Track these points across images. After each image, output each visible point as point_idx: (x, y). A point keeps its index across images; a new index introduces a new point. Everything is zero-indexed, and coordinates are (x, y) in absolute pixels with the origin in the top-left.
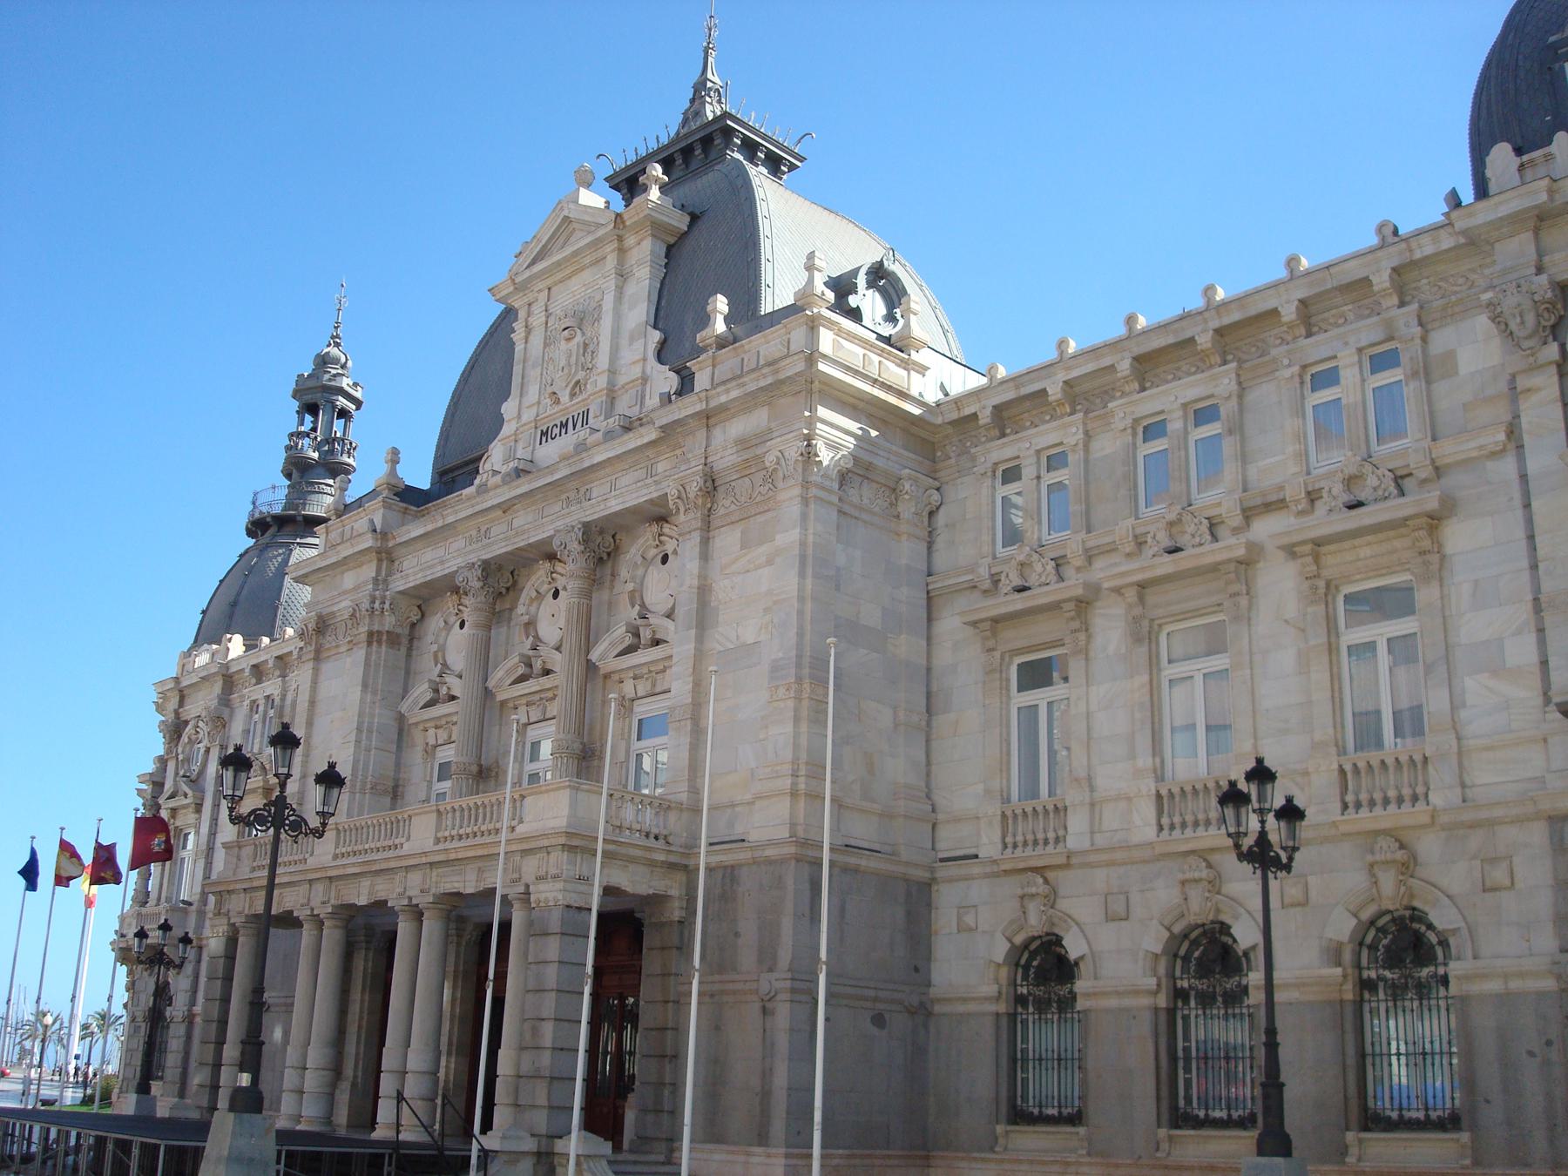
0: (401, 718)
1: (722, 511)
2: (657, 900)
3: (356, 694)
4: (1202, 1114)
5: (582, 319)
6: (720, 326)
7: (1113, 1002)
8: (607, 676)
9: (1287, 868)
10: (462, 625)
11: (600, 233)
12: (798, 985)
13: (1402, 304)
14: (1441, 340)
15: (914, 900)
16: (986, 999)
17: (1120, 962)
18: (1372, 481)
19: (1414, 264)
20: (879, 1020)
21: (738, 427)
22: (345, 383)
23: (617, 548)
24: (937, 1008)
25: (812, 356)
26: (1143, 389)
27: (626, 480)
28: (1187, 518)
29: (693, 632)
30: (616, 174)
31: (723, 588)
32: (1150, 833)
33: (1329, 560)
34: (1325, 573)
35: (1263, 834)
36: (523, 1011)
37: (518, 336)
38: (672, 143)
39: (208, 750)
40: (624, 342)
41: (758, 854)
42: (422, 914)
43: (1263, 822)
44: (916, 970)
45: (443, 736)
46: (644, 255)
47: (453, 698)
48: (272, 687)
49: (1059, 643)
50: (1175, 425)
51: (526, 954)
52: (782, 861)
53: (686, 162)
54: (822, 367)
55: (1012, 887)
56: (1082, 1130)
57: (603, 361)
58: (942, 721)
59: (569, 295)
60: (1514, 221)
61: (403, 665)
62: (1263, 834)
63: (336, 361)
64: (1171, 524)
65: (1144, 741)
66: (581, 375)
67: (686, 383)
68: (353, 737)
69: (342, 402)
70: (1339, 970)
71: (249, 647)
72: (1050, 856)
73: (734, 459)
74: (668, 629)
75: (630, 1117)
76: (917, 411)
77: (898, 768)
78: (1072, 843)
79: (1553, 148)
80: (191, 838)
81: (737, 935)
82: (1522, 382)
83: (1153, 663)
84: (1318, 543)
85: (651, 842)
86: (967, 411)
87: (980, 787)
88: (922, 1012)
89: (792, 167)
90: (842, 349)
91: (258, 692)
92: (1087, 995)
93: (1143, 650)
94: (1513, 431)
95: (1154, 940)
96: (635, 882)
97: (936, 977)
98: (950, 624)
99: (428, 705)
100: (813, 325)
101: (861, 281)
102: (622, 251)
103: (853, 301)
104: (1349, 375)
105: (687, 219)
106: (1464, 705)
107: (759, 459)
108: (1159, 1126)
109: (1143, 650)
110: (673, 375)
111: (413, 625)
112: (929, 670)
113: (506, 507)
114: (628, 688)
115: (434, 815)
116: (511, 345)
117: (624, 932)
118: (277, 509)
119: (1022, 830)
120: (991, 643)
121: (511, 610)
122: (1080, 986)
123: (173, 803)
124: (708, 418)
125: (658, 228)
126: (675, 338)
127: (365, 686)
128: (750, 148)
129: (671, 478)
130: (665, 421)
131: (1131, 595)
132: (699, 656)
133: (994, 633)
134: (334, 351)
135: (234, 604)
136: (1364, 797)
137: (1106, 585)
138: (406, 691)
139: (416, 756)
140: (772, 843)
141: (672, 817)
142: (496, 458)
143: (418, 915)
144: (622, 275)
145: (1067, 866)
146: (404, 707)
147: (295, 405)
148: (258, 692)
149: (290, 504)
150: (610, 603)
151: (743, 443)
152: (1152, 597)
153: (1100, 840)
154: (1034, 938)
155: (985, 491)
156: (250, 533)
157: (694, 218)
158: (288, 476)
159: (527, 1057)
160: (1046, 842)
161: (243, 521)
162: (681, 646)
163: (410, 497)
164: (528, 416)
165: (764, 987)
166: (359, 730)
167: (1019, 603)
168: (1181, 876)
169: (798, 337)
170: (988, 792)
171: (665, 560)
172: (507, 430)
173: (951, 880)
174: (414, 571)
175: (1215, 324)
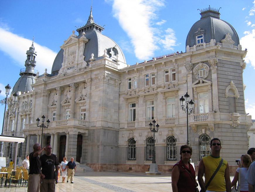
0: (48, 107)
1: (93, 83)
2: (85, 133)
3: (42, 104)
4: (170, 159)
5: (74, 53)
6: (93, 58)
7: (140, 146)
8: (77, 103)
9: (157, 132)
10: (56, 94)
11: (76, 41)
12: (102, 144)
13: (176, 64)
14: (180, 69)
15: (117, 132)
16: (125, 145)
17: (141, 142)
18: (171, 85)
19: (177, 59)
20: (112, 148)
21: (95, 73)
22: (34, 52)
23: (78, 86)
24: (119, 147)
25: (105, 65)
26: (146, 71)
27: (80, 77)
28: (150, 88)
29: (89, 99)
30: (78, 30)
31: (93, 93)
32: (145, 126)
33: (166, 94)
34: (166, 96)
35: (154, 128)
36: (68, 147)
37: (64, 54)
38: (85, 26)
39: (16, 109)
40: (79, 57)
41: (97, 128)
42: (54, 135)
43: (154, 127)
44: (117, 142)
45: (54, 110)
46: (82, 45)
47: (55, 105)
48: (26, 100)
49: (135, 102)
50: (149, 76)
51: (69, 140)
52: (100, 129)
53: (88, 29)
54: (106, 66)
55: (129, 132)
56: (136, 161)
57: (76, 59)
58: (121, 111)
59: (72, 49)
60: (188, 56)
61: (48, 99)
62: (154, 128)
63: (33, 48)
64: (148, 88)
65: (144, 115)
66: (73, 61)
67: (88, 65)
68: (41, 110)
69: (34, 55)
70: (164, 143)
71: (22, 93)
72: (133, 128)
73: (94, 77)
74: (86, 98)
75: (81, 160)
76: (117, 70)
77: (115, 117)
78: (135, 127)
79: (194, 47)
80: (14, 121)
81: (95, 138)
82: (188, 75)
83: (146, 105)
84: (165, 92)
85: (84, 126)
86: (125, 71)
87: (125, 119)
88: (117, 147)
89: (102, 30)
90: (109, 63)
91: (24, 100)
92: (137, 145)
93: (145, 104)
94: (187, 81)
95: (145, 139)
96: (82, 131)
97: (119, 143)
98: (122, 99)
99: (52, 105)
100: (105, 60)
101: (112, 50)
102: (79, 44)
103: (110, 53)
104: (169, 72)
105: (88, 40)
106: (179, 113)
107: (98, 77)
108: (145, 160)
109: (145, 104)
110: (86, 63)
111: (49, 94)
112: (119, 104)
113: (63, 79)
114: (80, 105)
115: (56, 122)
116: (63, 55)
117: (80, 137)
118: (24, 72)
119: (130, 125)
120: (127, 101)
121: (63, 93)
122: (136, 144)
123: (11, 116)
124: (91, 71)
125: (84, 41)
126: (87, 60)
127: (43, 102)
128: (97, 28)
129: (86, 78)
130: (86, 71)
131: (143, 97)
132: (90, 102)
133: (127, 100)
134: (33, 47)
135: (19, 86)
136: (168, 123)
137: (140, 95)
138: (48, 104)
139: (50, 112)
140: (99, 127)
141: (87, 123)
142: (61, 71)
143: (54, 135)
144: (79, 47)
145: (135, 130)
146: (48, 106)
147: (27, 55)
148: (24, 100)
149: (26, 71)
150: (77, 93)
151: (96, 75)
152: (146, 97)
153: (139, 127)
154: (131, 138)
155: (127, 81)
156: (20, 75)
157: (89, 40)
158: (26, 66)
159: (69, 153)
160: (133, 127)
161: (19, 73)
162: (87, 100)
163: (48, 75)
164: (66, 66)
165: (98, 144)
166: (42, 109)
167: (130, 97)
168: (148, 131)
169: (103, 61)
170: (126, 120)
171: (85, 88)
172: (63, 67)
173: (121, 131)
174: (50, 87)
175: (155, 63)
